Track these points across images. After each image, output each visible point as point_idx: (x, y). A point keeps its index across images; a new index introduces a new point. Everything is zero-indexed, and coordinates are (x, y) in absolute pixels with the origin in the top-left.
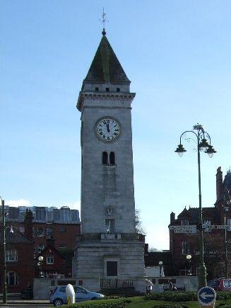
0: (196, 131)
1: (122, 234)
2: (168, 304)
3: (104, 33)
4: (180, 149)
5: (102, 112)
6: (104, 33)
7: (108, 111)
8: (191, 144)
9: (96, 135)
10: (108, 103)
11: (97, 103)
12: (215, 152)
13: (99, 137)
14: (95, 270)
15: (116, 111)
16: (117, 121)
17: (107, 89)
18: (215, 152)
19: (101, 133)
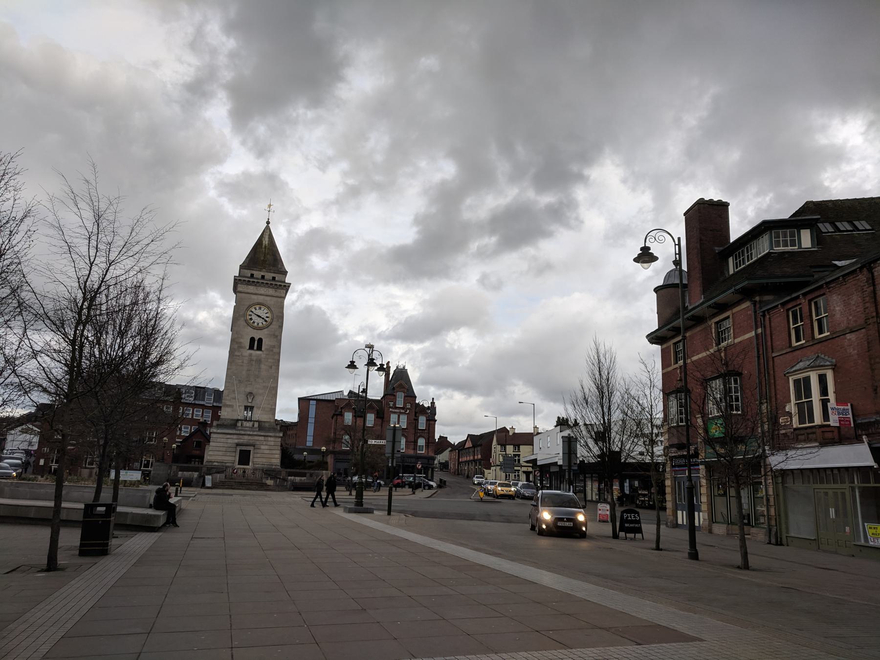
0: (368, 350)
1: (203, 485)
2: (794, 295)
3: (268, 223)
4: (352, 365)
5: (261, 299)
6: (268, 223)
7: (261, 298)
8: (361, 364)
9: (246, 321)
10: (262, 290)
11: (251, 289)
12: (177, 526)
13: (249, 323)
14: (274, 452)
15: (268, 298)
16: (268, 308)
17: (263, 277)
18: (636, 260)
19: (251, 319)
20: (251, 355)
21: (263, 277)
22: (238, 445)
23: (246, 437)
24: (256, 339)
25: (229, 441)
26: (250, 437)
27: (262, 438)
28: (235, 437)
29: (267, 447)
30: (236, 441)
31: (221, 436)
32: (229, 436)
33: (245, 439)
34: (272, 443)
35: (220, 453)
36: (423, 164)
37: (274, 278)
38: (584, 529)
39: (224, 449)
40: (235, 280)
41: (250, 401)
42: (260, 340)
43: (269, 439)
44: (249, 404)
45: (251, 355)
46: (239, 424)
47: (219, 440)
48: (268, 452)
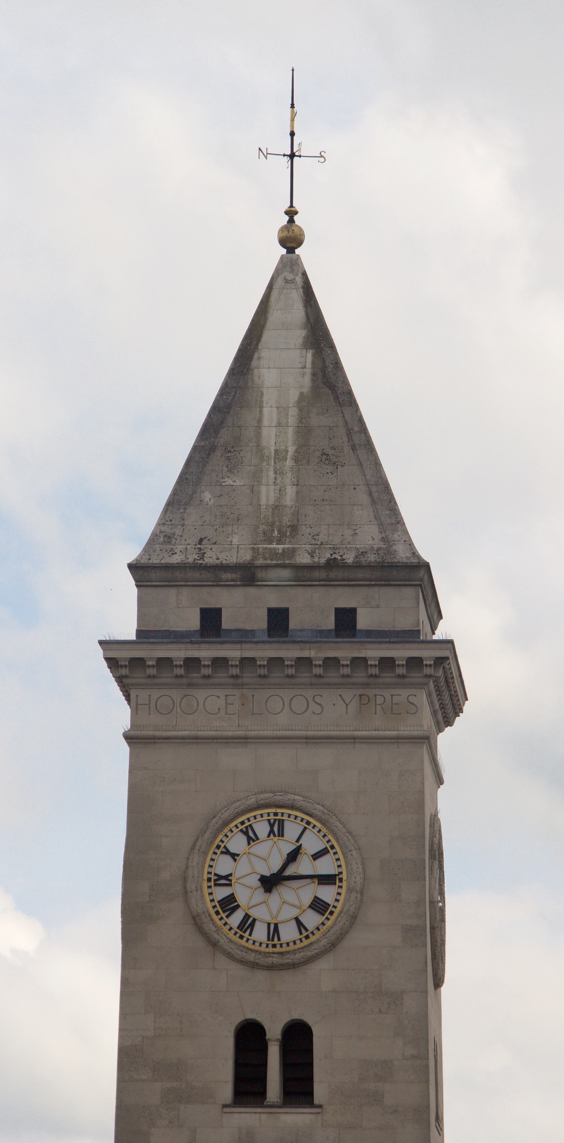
3: (291, 240)
6: (291, 240)
10: (283, 709)
15: (322, 758)
17: (278, 620)
19: (229, 904)
21: (278, 620)
24: (274, 1032)
37: (346, 619)
42: (298, 1037)
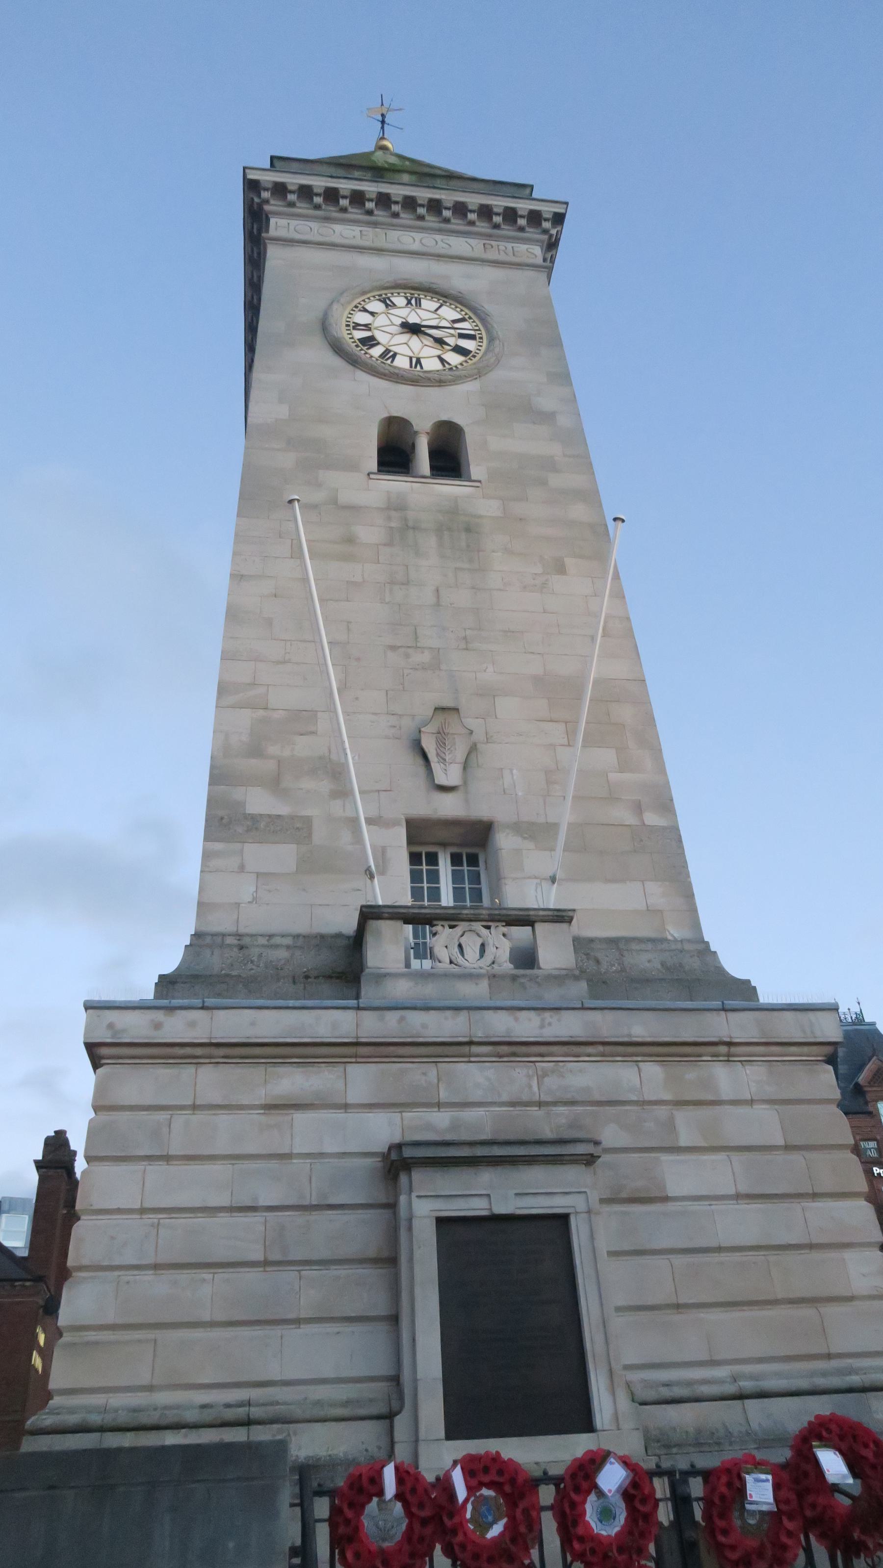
20: (396, 506)
22: (398, 1164)
23: (476, 1077)
25: (306, 1132)
26: (519, 1079)
27: (649, 1078)
28: (360, 1080)
29: (719, 1174)
30: (382, 1130)
31: (209, 1081)
32: (292, 1081)
33: (478, 1097)
34: (766, 1125)
35: (207, 1294)
36: (341, 1454)
38: (37, 1361)
39: (246, 1237)
40: (252, 186)
41: (448, 773)
43: (726, 1078)
44: (448, 807)
45: (396, 506)
46: (388, 949)
47: (180, 1134)
48: (743, 1225)
